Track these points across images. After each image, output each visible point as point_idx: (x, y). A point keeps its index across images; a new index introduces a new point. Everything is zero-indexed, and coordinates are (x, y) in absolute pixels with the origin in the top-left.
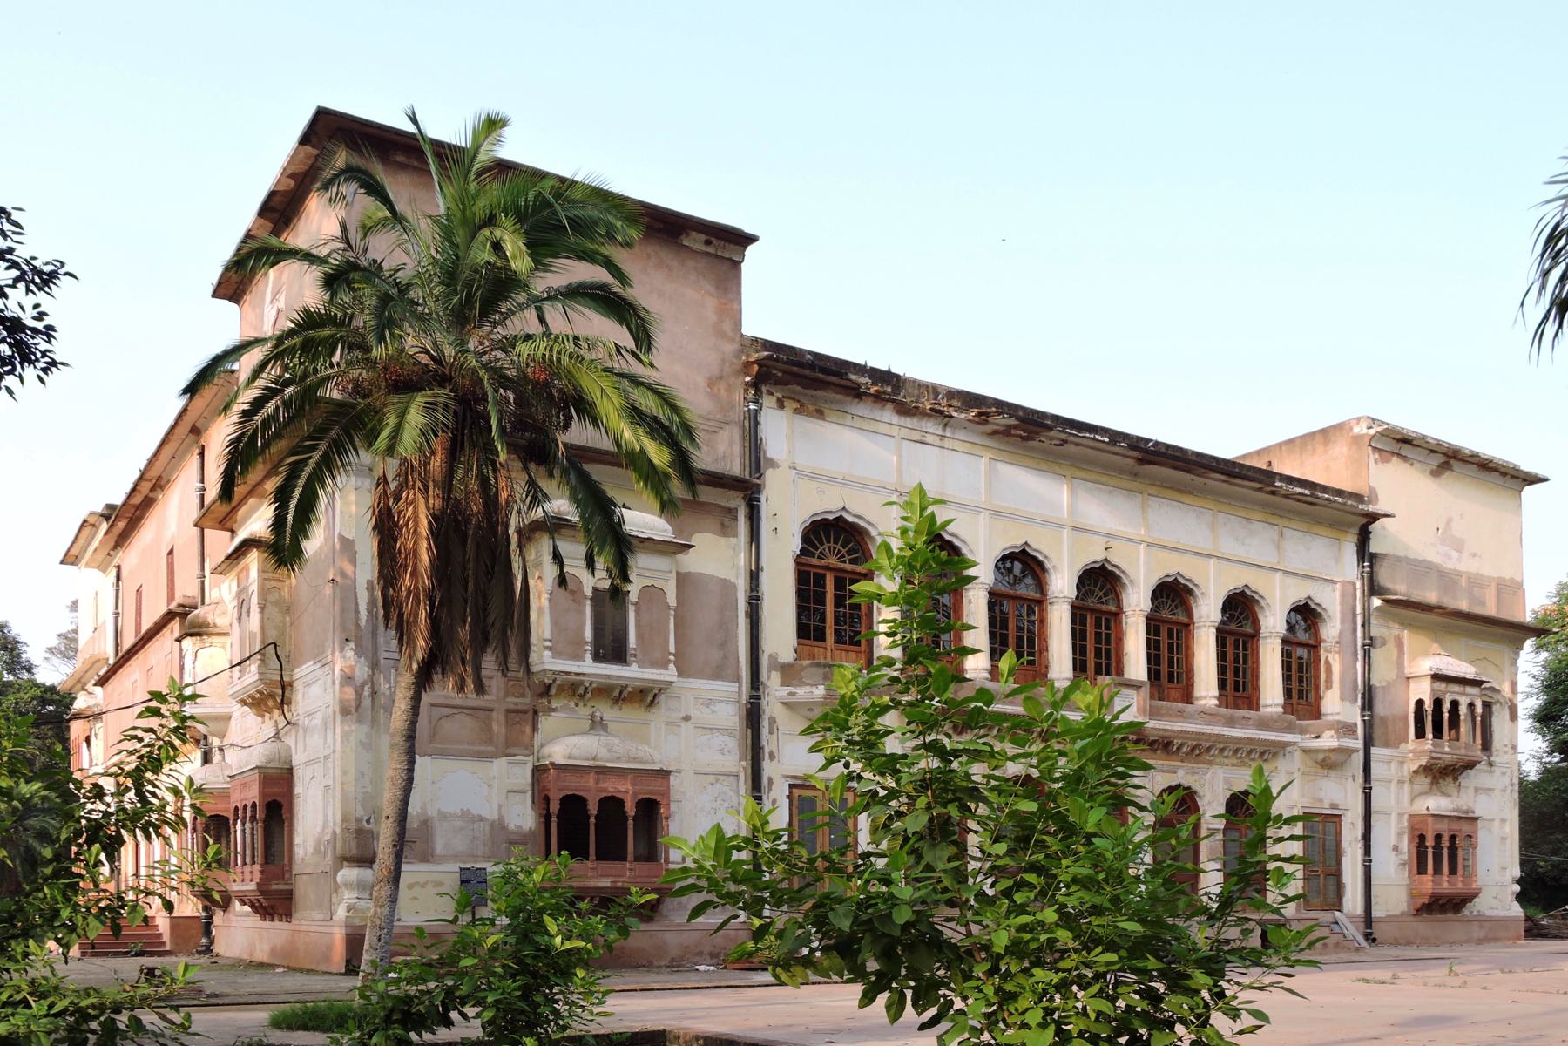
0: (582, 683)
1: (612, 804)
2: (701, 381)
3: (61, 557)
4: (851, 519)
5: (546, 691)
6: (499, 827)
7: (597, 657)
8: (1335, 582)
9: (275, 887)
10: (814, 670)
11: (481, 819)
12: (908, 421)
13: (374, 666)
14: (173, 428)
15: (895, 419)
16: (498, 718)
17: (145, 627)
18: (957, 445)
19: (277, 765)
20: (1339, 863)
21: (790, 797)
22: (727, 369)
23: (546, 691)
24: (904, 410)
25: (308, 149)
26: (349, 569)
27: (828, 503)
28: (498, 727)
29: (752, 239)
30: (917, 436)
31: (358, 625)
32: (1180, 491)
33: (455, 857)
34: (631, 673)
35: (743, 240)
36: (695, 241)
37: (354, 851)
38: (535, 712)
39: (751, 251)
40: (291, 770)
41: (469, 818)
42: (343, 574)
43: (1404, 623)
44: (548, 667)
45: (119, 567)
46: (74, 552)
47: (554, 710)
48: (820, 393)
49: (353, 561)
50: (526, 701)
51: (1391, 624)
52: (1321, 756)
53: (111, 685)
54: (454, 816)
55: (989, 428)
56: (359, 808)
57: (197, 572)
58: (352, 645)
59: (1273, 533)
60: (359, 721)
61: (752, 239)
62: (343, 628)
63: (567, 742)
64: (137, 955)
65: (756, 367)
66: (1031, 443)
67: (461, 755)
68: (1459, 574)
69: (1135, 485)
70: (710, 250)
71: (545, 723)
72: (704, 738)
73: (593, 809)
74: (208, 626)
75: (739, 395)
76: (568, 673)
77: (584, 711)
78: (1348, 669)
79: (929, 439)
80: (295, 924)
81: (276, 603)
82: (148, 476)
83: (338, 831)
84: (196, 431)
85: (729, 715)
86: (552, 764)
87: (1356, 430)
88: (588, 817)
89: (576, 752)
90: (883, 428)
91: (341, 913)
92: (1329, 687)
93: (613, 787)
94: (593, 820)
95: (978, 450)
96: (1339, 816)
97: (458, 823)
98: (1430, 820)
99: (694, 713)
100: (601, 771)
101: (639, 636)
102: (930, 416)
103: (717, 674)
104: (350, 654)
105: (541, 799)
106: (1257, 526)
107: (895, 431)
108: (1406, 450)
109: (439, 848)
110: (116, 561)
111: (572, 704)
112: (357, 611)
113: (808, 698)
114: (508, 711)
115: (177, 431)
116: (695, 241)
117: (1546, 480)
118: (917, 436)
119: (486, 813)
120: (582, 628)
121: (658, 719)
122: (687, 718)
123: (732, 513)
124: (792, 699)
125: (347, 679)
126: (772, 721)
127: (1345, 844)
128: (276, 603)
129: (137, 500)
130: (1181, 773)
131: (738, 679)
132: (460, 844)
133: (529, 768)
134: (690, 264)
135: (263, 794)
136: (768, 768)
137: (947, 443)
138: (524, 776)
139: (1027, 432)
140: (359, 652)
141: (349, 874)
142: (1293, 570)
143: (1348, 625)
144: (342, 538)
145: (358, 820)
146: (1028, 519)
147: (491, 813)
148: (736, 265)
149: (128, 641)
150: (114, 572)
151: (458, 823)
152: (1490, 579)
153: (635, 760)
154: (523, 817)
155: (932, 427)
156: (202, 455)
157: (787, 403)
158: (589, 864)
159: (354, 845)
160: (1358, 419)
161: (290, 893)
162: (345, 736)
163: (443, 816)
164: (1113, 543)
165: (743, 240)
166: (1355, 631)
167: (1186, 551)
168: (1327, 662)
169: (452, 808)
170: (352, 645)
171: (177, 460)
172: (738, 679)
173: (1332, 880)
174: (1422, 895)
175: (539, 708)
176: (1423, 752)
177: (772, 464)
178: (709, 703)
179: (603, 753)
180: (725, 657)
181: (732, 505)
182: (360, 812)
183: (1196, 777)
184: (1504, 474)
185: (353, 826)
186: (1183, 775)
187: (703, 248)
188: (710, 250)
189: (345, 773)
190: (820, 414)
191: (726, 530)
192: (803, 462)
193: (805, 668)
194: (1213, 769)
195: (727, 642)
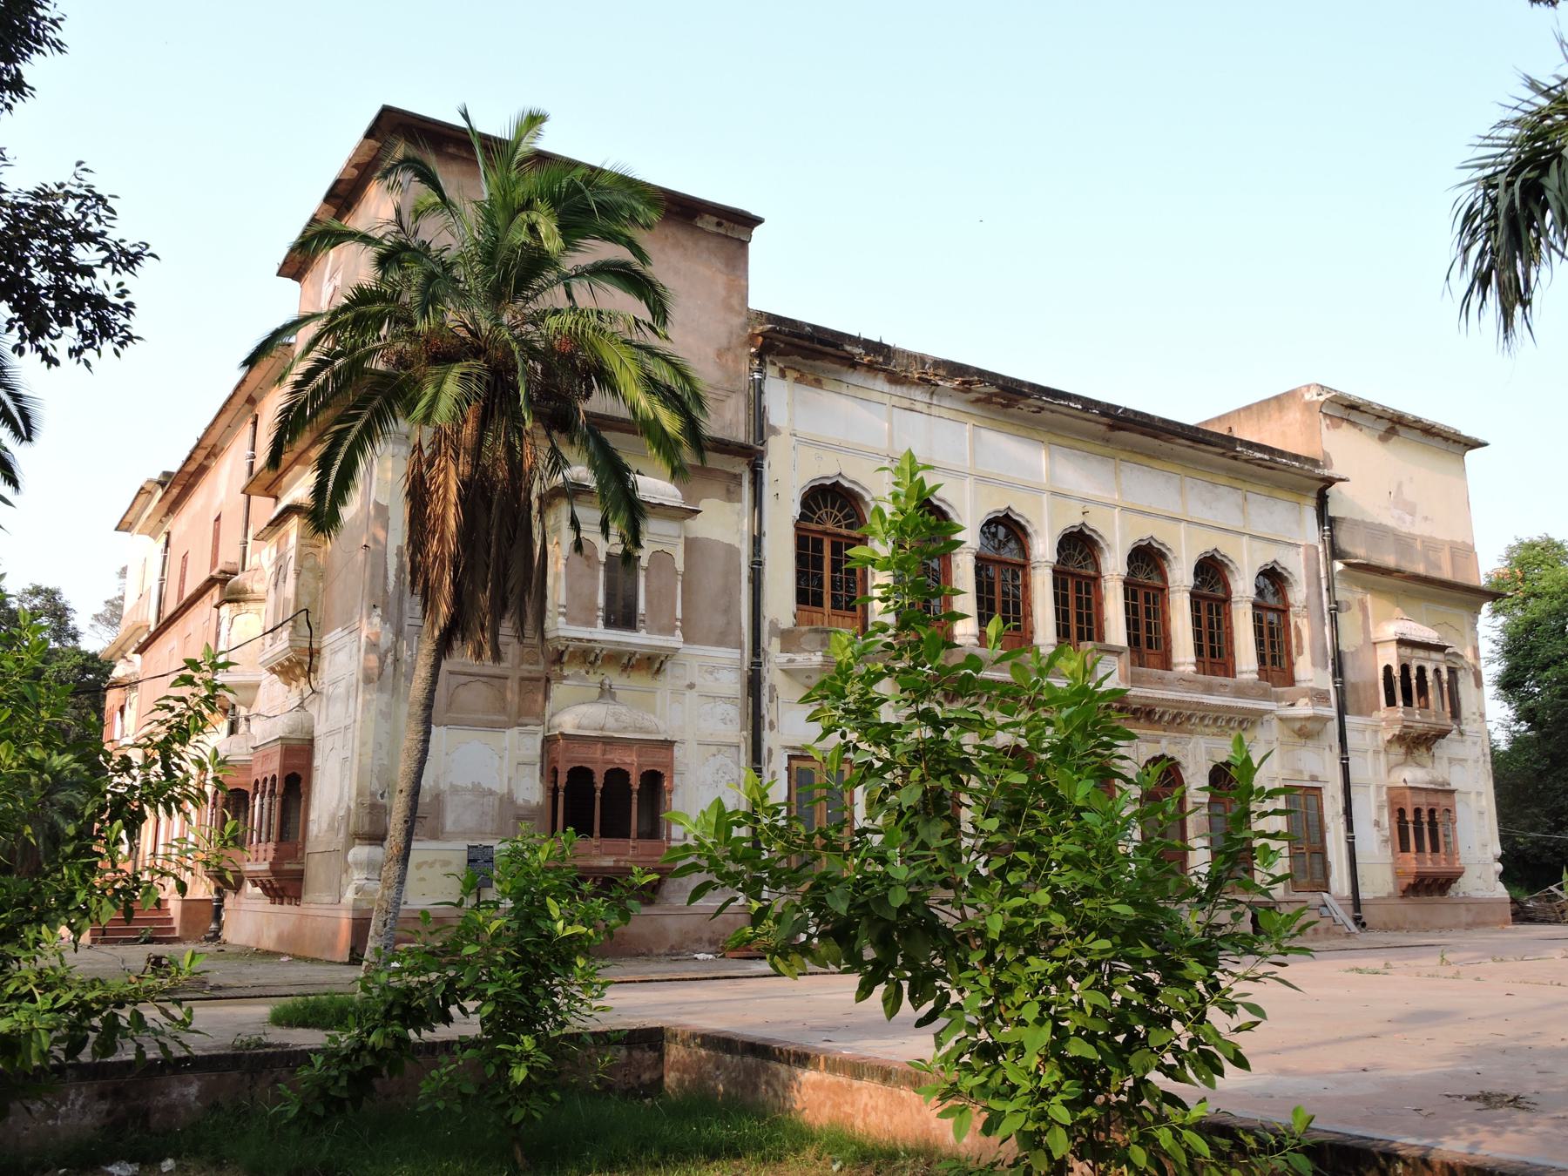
0: (593, 649)
1: (617, 776)
2: (711, 353)
4: (846, 484)
5: (558, 658)
6: (507, 801)
7: (609, 624)
8: (1298, 546)
10: (812, 636)
11: (491, 793)
12: (898, 390)
13: (399, 633)
15: (887, 387)
16: (512, 686)
18: (944, 413)
20: (1323, 840)
21: (789, 769)
22: (734, 341)
23: (558, 658)
24: (895, 379)
25: (372, 142)
26: (381, 534)
27: (824, 468)
28: (512, 696)
30: (906, 403)
31: (386, 591)
32: (1150, 457)
33: (463, 834)
34: (640, 639)
36: (707, 223)
38: (548, 680)
40: (312, 740)
41: (481, 792)
42: (376, 540)
43: (1367, 588)
44: (562, 633)
45: (168, 534)
47: (565, 678)
48: (818, 363)
49: (386, 528)
50: (539, 669)
51: (1355, 588)
52: (1297, 725)
54: (465, 789)
58: (379, 611)
59: (1236, 497)
60: (381, 690)
63: (577, 711)
64: (146, 942)
67: (474, 725)
68: (1414, 538)
69: (1108, 451)
70: (722, 231)
71: (557, 691)
73: (599, 782)
74: (246, 592)
76: (580, 640)
77: (594, 679)
78: (1317, 634)
79: (918, 406)
81: (311, 570)
82: (204, 444)
84: (252, 401)
85: (732, 683)
86: (562, 734)
87: (1307, 397)
89: (585, 722)
90: (875, 396)
91: (349, 896)
92: (1300, 653)
93: (620, 758)
94: (598, 794)
95: (962, 417)
96: (1319, 789)
97: (469, 797)
99: (698, 681)
100: (609, 742)
101: (648, 602)
103: (723, 639)
104: (376, 620)
106: (1222, 490)
107: (886, 399)
108: (1354, 416)
110: (166, 529)
111: (583, 672)
112: (386, 577)
114: (523, 679)
115: (234, 401)
117: (1486, 444)
118: (906, 403)
121: (664, 687)
122: (691, 686)
123: (737, 478)
125: (373, 646)
126: (773, 688)
127: (1327, 819)
128: (311, 570)
129: (192, 467)
130: (1164, 742)
131: (740, 646)
132: (470, 820)
133: (540, 738)
135: (283, 767)
136: (769, 739)
137: (935, 410)
139: (1008, 400)
142: (1262, 535)
143: (1314, 589)
144: (377, 504)
145: (373, 794)
146: (838, 448)
147: (500, 787)
148: (744, 244)
149: (170, 607)
150: (163, 539)
151: (469, 797)
152: (1444, 542)
153: (641, 730)
154: (532, 791)
155: (919, 395)
156: (255, 424)
157: (788, 372)
158: (594, 842)
159: (367, 820)
160: (1308, 387)
162: (366, 704)
163: (455, 790)
164: (1089, 507)
166: (1320, 595)
167: (1157, 515)
168: (1297, 627)
169: (465, 781)
170: (379, 611)
171: (232, 428)
172: (740, 646)
173: (1317, 858)
174: (1406, 874)
175: (552, 676)
176: (1395, 721)
177: (775, 431)
178: (712, 670)
179: (611, 722)
180: (728, 623)
181: (737, 471)
183: (1179, 747)
184: (1446, 439)
185: (367, 801)
186: (1166, 745)
187: (713, 229)
188: (722, 231)
189: (363, 744)
190: (818, 383)
191: (731, 495)
192: (803, 429)
193: (803, 634)
194: (1195, 738)
195: (730, 609)
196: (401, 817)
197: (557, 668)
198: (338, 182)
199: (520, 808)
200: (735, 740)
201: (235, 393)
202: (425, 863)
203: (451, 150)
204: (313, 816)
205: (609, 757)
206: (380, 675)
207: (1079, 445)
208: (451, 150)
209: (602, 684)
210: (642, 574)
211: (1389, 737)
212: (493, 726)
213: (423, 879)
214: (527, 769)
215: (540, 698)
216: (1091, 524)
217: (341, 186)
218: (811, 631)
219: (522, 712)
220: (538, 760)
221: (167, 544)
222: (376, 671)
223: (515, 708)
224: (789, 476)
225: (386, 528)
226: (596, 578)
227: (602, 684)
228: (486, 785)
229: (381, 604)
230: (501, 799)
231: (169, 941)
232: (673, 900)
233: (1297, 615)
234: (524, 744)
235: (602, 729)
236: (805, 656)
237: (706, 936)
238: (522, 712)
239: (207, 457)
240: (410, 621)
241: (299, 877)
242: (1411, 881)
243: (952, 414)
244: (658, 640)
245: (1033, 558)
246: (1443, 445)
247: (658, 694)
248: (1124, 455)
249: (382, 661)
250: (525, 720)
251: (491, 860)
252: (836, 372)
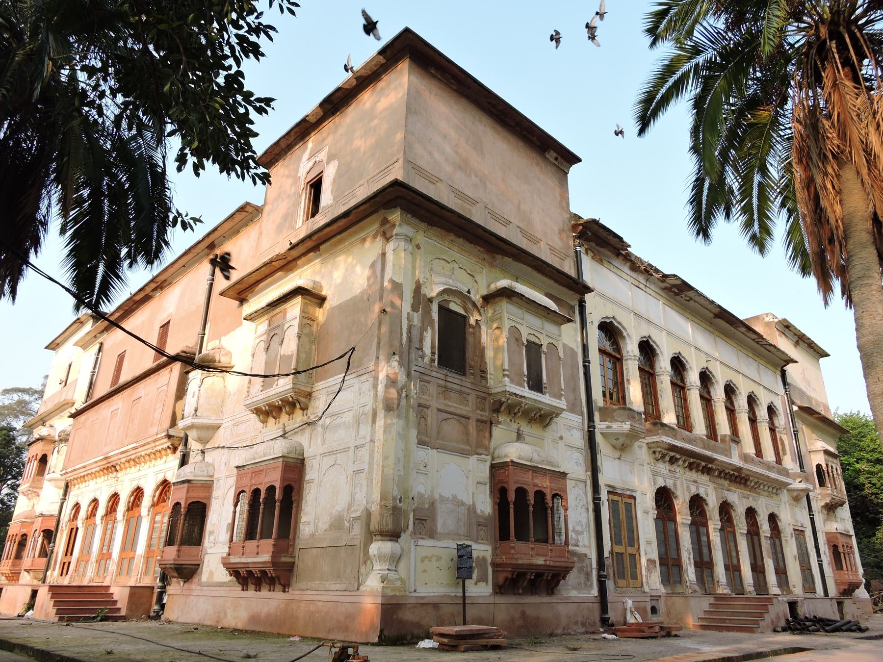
0: (520, 404)
2: (556, 229)
3: (47, 344)
4: (616, 324)
5: (497, 407)
6: (472, 510)
7: (530, 388)
9: (283, 559)
10: (621, 412)
13: (409, 375)
14: (199, 242)
15: (629, 272)
16: (472, 426)
17: (124, 378)
19: (293, 456)
21: (608, 500)
22: (566, 228)
23: (497, 407)
26: (398, 302)
29: (577, 160)
30: (637, 283)
31: (401, 343)
33: (449, 535)
34: (545, 399)
35: (574, 159)
36: (551, 155)
37: (390, 527)
38: (491, 423)
39: (574, 170)
40: (303, 460)
42: (393, 305)
44: (508, 389)
45: (101, 344)
46: (58, 341)
47: (499, 423)
48: (602, 249)
49: (401, 297)
52: (795, 494)
53: (82, 418)
55: (665, 285)
56: (395, 488)
57: (201, 331)
58: (397, 357)
60: (399, 416)
61: (577, 160)
62: (391, 345)
64: (101, 620)
65: (581, 227)
66: (678, 298)
69: (710, 329)
71: (497, 431)
72: (569, 453)
74: (215, 361)
75: (571, 243)
76: (516, 395)
77: (515, 426)
78: (791, 445)
79: (642, 286)
80: (293, 594)
81: (307, 335)
82: (157, 280)
83: (375, 508)
86: (512, 461)
87: (767, 319)
88: (528, 506)
89: (523, 454)
91: (373, 583)
92: (785, 454)
94: (531, 508)
95: (658, 296)
96: (803, 531)
98: (839, 536)
99: (564, 435)
100: (535, 470)
102: (642, 273)
104: (395, 364)
105: (500, 493)
107: (628, 278)
108: (787, 332)
109: (440, 528)
110: (100, 340)
111: (508, 420)
113: (620, 430)
114: (478, 421)
115: (199, 246)
116: (551, 155)
117: (796, 362)
118: (637, 283)
119: (465, 500)
120: (522, 365)
124: (609, 431)
125: (392, 382)
128: (307, 335)
129: (138, 298)
131: (582, 415)
133: (488, 464)
134: (549, 167)
135: (283, 479)
137: (648, 290)
138: (484, 472)
140: (401, 364)
141: (378, 547)
144: (392, 281)
145: (394, 499)
147: (468, 501)
148: (566, 174)
149: (101, 390)
154: (485, 505)
155: (642, 279)
159: (390, 521)
160: (767, 314)
161: (292, 564)
163: (442, 499)
165: (574, 159)
169: (447, 494)
170: (397, 357)
172: (582, 415)
173: (761, 575)
174: (843, 583)
175: (493, 420)
176: (827, 495)
179: (536, 457)
181: (572, 303)
182: (396, 492)
184: (815, 350)
185: (390, 504)
187: (553, 160)
189: (385, 458)
195: (575, 390)
196: (400, 520)
197: (495, 415)
198: (339, 90)
199: (478, 516)
200: (583, 477)
201: (203, 239)
202: (426, 557)
203: (432, 71)
204: (304, 519)
205: (536, 481)
206: (399, 405)
207: (701, 323)
208: (432, 71)
209: (519, 430)
210: (543, 356)
211: (823, 504)
212: (465, 453)
213: (425, 571)
214: (481, 487)
215: (487, 434)
216: (711, 369)
217: (338, 94)
218: (619, 408)
219: (479, 445)
220: (488, 481)
221: (100, 350)
222: (396, 402)
223: (474, 442)
224: (597, 309)
225: (401, 297)
226: (521, 354)
227: (519, 430)
228: (460, 497)
229: (405, 352)
230: (469, 509)
231: (116, 619)
232: (562, 592)
233: (780, 433)
234: (478, 469)
235: (531, 461)
236: (619, 424)
237: (580, 619)
238: (479, 445)
239: (155, 289)
240: (415, 368)
241: (290, 568)
242: (846, 587)
243: (653, 294)
244: (555, 402)
245: (688, 383)
246: (813, 353)
247: (545, 441)
248: (717, 333)
249: (400, 394)
250: (480, 451)
251: (470, 557)
252: (609, 257)
